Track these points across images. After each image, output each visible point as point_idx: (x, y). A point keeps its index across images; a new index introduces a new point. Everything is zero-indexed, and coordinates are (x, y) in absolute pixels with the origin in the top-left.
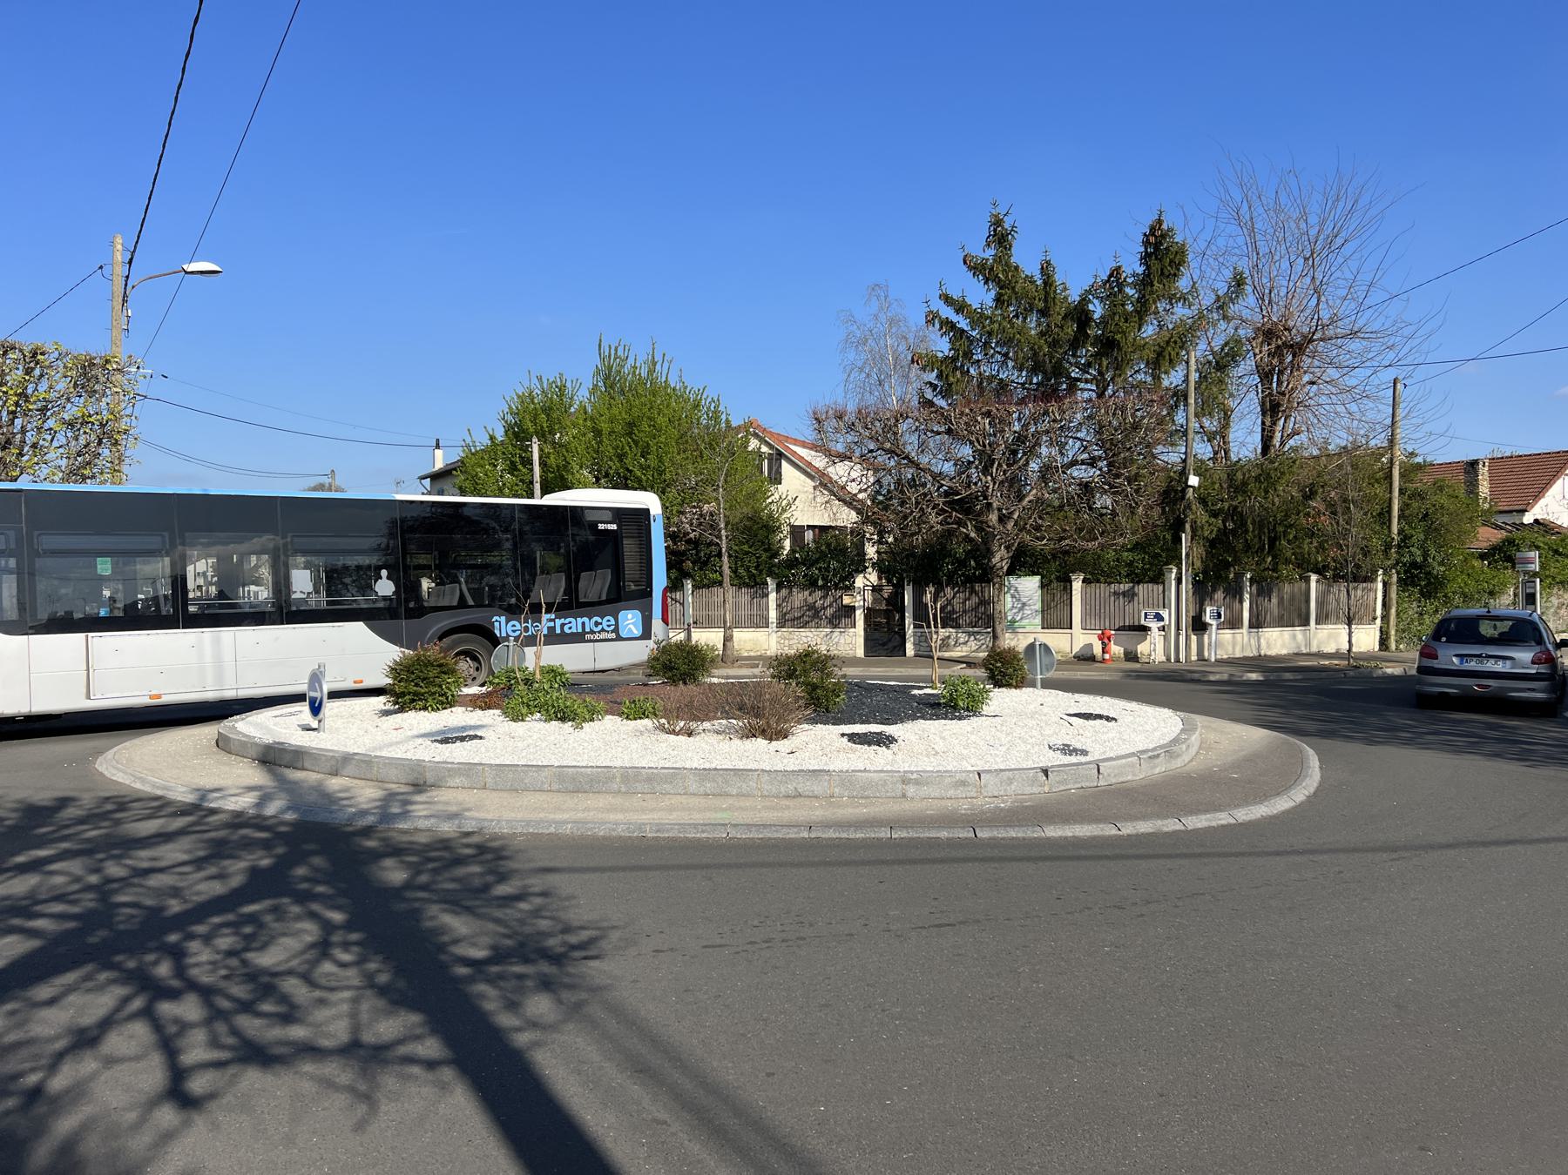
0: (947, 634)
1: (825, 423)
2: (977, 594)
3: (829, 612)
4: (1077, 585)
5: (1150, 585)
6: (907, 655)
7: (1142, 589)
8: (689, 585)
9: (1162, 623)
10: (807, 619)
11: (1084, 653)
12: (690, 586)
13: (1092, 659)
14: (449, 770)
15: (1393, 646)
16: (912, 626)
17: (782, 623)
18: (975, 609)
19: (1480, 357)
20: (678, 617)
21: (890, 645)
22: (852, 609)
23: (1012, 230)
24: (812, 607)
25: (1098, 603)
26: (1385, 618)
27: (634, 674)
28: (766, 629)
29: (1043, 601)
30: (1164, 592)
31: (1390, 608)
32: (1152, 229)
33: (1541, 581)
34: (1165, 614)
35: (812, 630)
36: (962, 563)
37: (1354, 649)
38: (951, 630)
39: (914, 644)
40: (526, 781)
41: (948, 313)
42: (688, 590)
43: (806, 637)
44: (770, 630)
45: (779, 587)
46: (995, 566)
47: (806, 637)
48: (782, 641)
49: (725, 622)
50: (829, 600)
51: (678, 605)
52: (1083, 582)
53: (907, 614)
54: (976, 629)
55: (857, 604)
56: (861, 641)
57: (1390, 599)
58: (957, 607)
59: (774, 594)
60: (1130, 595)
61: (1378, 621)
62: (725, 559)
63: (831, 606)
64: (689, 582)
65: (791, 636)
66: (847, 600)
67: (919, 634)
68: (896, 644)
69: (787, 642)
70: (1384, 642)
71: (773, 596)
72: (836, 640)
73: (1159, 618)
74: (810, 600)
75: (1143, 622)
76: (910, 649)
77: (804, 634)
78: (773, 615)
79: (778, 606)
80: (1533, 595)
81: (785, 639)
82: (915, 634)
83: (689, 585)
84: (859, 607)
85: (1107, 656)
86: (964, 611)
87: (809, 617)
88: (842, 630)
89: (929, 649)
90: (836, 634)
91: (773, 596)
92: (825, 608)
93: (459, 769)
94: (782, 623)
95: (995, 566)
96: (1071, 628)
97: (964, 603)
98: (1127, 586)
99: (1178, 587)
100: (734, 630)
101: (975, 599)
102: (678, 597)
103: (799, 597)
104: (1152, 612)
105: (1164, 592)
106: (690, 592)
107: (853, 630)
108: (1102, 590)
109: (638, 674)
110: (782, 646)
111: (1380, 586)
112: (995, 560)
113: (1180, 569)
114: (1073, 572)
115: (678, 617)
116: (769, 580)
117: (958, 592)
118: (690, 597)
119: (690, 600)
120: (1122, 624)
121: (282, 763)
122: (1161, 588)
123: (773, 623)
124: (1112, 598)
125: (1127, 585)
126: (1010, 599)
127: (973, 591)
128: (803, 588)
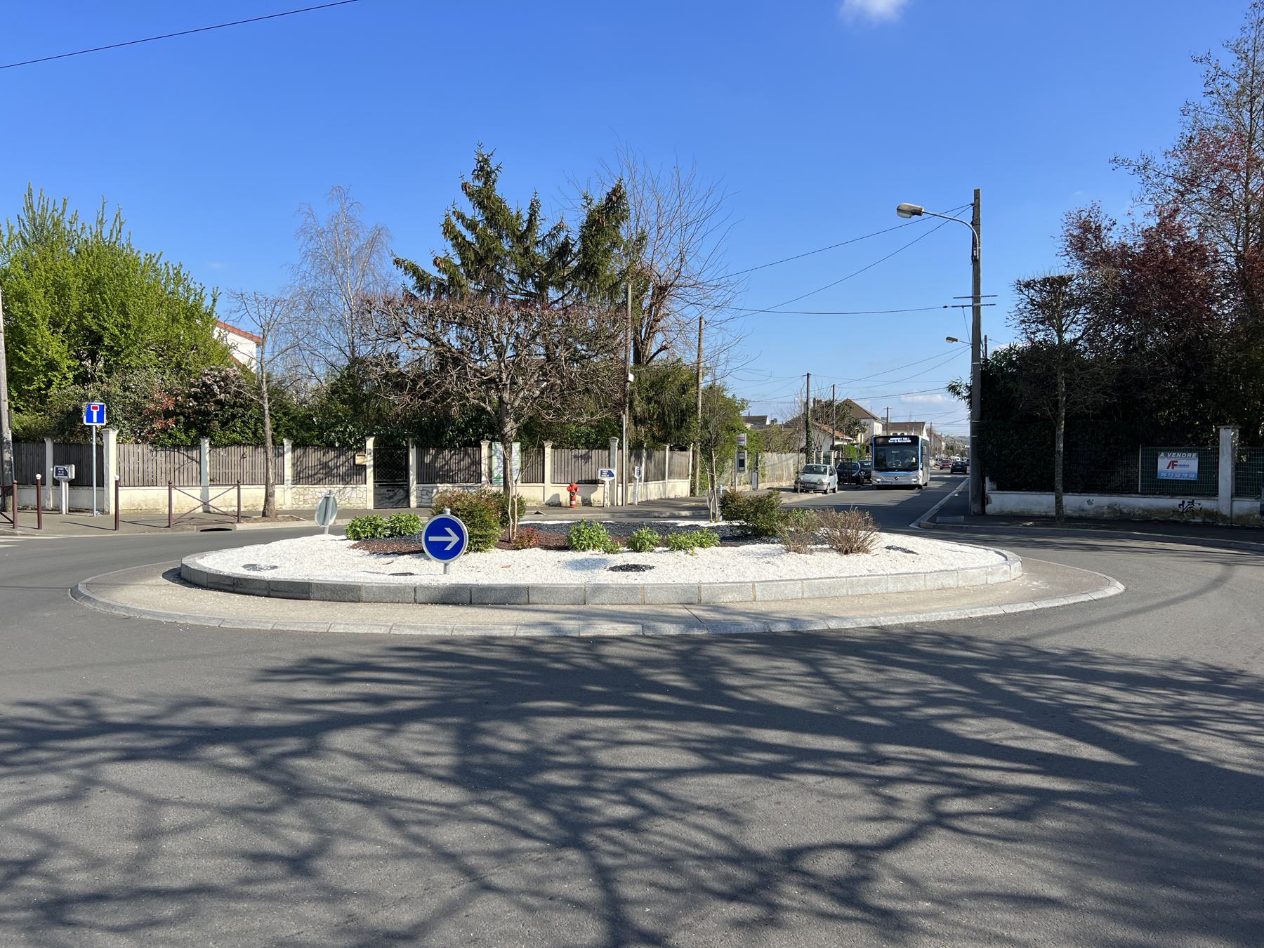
0: (445, 488)
1: (288, 297)
2: (469, 456)
3: (342, 470)
4: (548, 450)
5: (600, 451)
6: (411, 506)
7: (595, 454)
8: (206, 444)
9: (612, 478)
10: (321, 476)
11: (553, 500)
12: (207, 445)
13: (559, 505)
14: (722, 589)
15: (697, 494)
16: (415, 482)
17: (297, 480)
18: (468, 468)
19: (749, 312)
20: (194, 475)
21: (396, 499)
22: (364, 467)
23: (497, 169)
24: (325, 465)
25: (563, 463)
26: (694, 475)
27: (188, 530)
28: (282, 486)
29: (522, 462)
30: (609, 455)
31: (696, 468)
32: (615, 191)
33: (748, 453)
34: (615, 472)
35: (326, 486)
36: (462, 432)
37: (242, 509)
38: (448, 485)
39: (417, 497)
40: (786, 592)
41: (460, 227)
42: (205, 449)
43: (321, 492)
44: (285, 486)
45: (294, 449)
46: (506, 434)
47: (321, 492)
48: (297, 497)
49: (268, 479)
50: (342, 459)
51: (194, 463)
52: (552, 448)
53: (411, 472)
54: (469, 484)
55: (367, 464)
56: (371, 495)
57: (696, 463)
58: (453, 467)
59: (290, 453)
60: (586, 458)
61: (690, 477)
62: (267, 420)
63: (343, 465)
64: (206, 441)
65: (306, 492)
66: (359, 460)
67: (421, 489)
68: (400, 497)
69: (302, 497)
70: (692, 491)
71: (288, 456)
72: (348, 495)
73: (611, 474)
74: (324, 459)
75: (599, 477)
76: (413, 502)
77: (318, 490)
78: (288, 473)
79: (294, 465)
80: (743, 461)
81: (300, 494)
82: (417, 489)
83: (206, 444)
84: (370, 466)
85: (574, 503)
86: (459, 470)
87: (326, 474)
88: (354, 486)
89: (429, 501)
90: (348, 490)
91: (288, 456)
92: (338, 467)
93: (732, 587)
94: (297, 480)
95: (506, 434)
96: (543, 482)
97: (459, 463)
98: (584, 451)
99: (619, 454)
100: (276, 486)
101: (467, 461)
102: (194, 456)
103: (313, 457)
104: (606, 470)
105: (609, 455)
106: (207, 451)
107: (364, 486)
108: (566, 453)
109: (193, 530)
110: (297, 501)
111: (691, 453)
112: (507, 429)
113: (621, 439)
114: (546, 440)
115: (194, 475)
116: (285, 441)
117: (455, 454)
118: (208, 455)
119: (208, 459)
120: (580, 479)
121: (487, 601)
122: (607, 452)
123: (288, 480)
124: (573, 460)
125: (584, 451)
126: (496, 460)
127: (466, 454)
128: (318, 448)
